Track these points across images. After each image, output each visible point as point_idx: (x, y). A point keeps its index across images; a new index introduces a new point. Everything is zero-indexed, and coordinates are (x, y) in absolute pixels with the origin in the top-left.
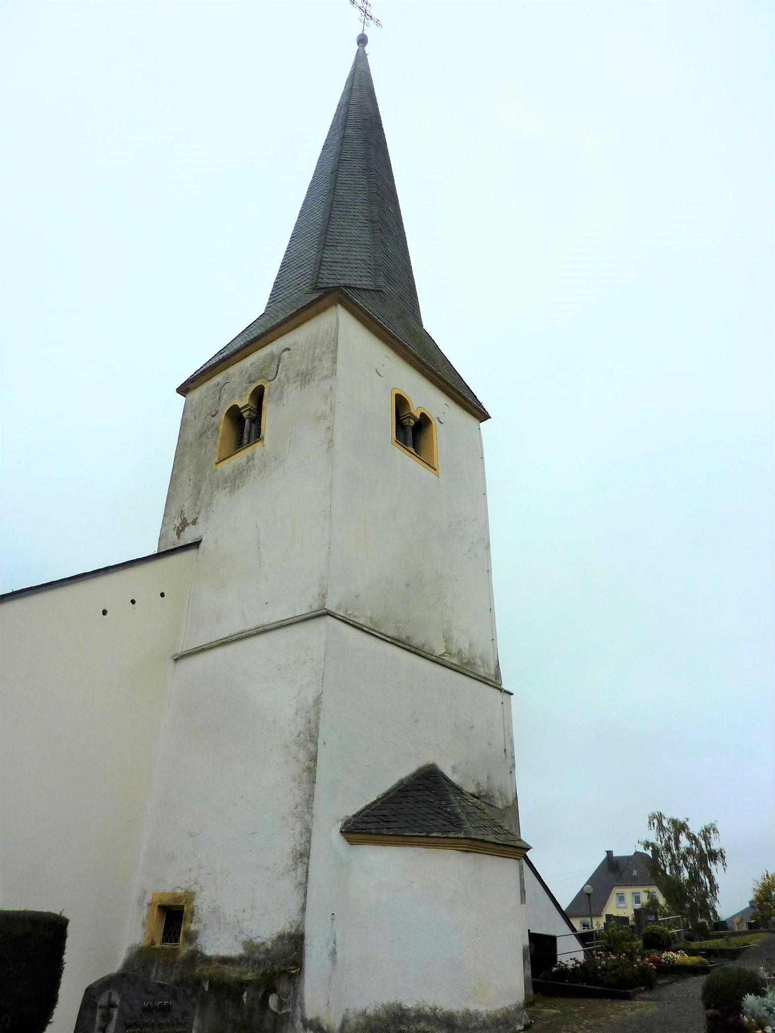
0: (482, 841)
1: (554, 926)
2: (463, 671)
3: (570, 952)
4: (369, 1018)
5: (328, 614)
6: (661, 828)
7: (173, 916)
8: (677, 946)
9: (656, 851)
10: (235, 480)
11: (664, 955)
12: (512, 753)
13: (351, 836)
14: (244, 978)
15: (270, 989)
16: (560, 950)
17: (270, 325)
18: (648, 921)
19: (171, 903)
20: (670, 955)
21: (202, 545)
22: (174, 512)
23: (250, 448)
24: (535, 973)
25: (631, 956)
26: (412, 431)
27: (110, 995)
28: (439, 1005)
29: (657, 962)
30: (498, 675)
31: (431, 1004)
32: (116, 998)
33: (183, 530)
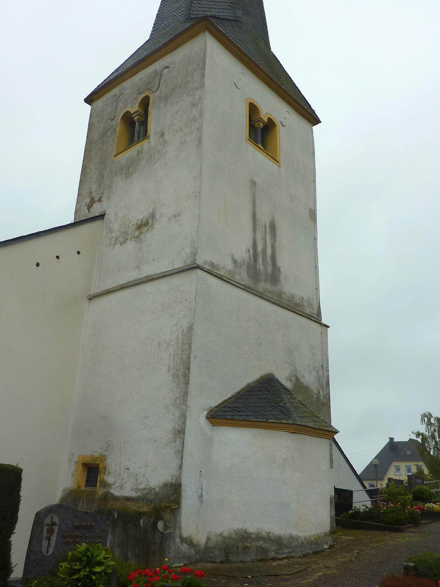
0: (305, 426)
1: (353, 485)
2: (295, 310)
3: (361, 501)
4: (225, 538)
5: (198, 267)
6: (429, 423)
7: (92, 470)
8: (436, 500)
9: (424, 439)
10: (129, 168)
11: (427, 505)
12: (328, 367)
13: (213, 420)
14: (141, 510)
15: (159, 518)
16: (354, 500)
17: (154, 48)
18: (416, 483)
19: (91, 462)
20: (431, 505)
21: (106, 217)
22: (85, 193)
23: (139, 144)
24: (337, 514)
25: (404, 505)
26: (262, 132)
27: (52, 517)
28: (272, 531)
29: (422, 509)
30: (319, 313)
31: (267, 531)
32: (56, 520)
33: (92, 206)
